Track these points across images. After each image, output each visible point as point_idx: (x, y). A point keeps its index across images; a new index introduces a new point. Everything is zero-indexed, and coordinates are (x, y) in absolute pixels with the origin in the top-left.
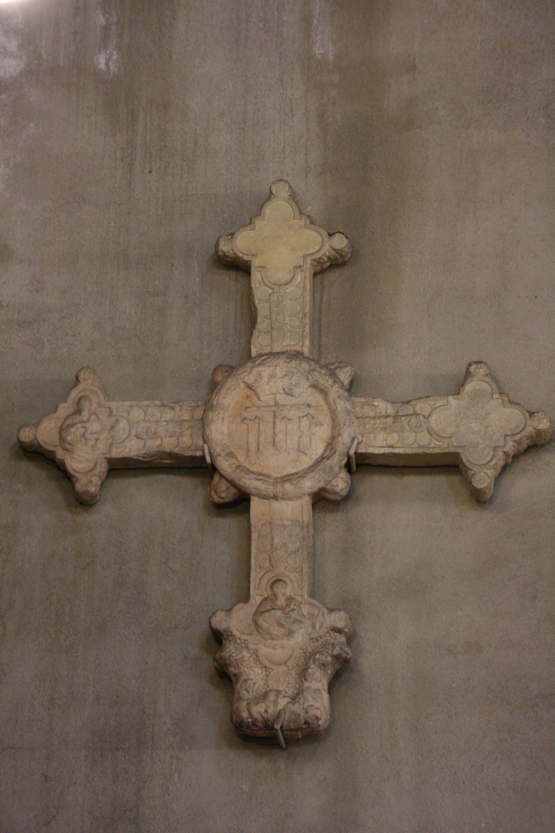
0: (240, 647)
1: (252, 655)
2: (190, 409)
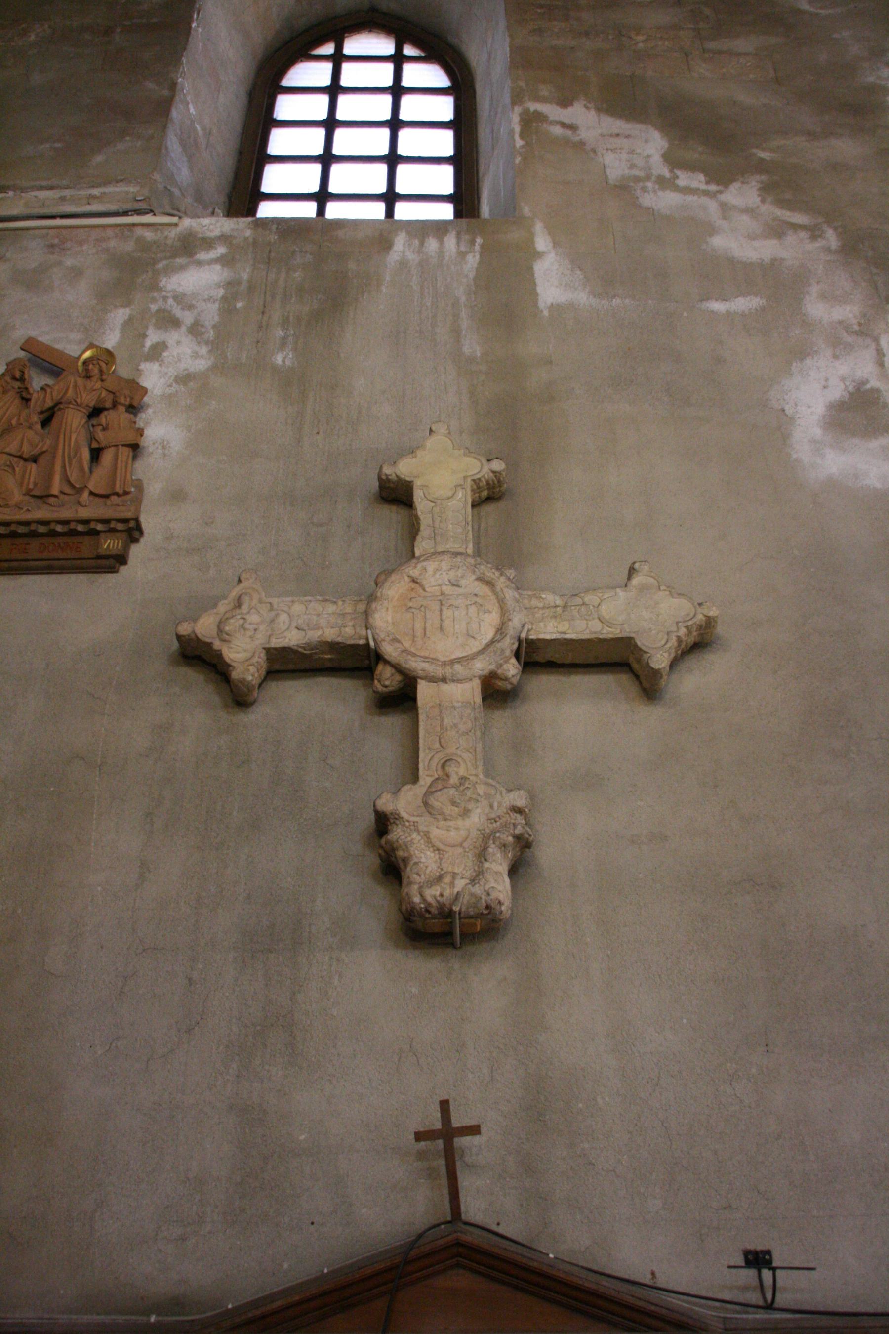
0: (409, 830)
1: (422, 838)
2: (353, 603)
